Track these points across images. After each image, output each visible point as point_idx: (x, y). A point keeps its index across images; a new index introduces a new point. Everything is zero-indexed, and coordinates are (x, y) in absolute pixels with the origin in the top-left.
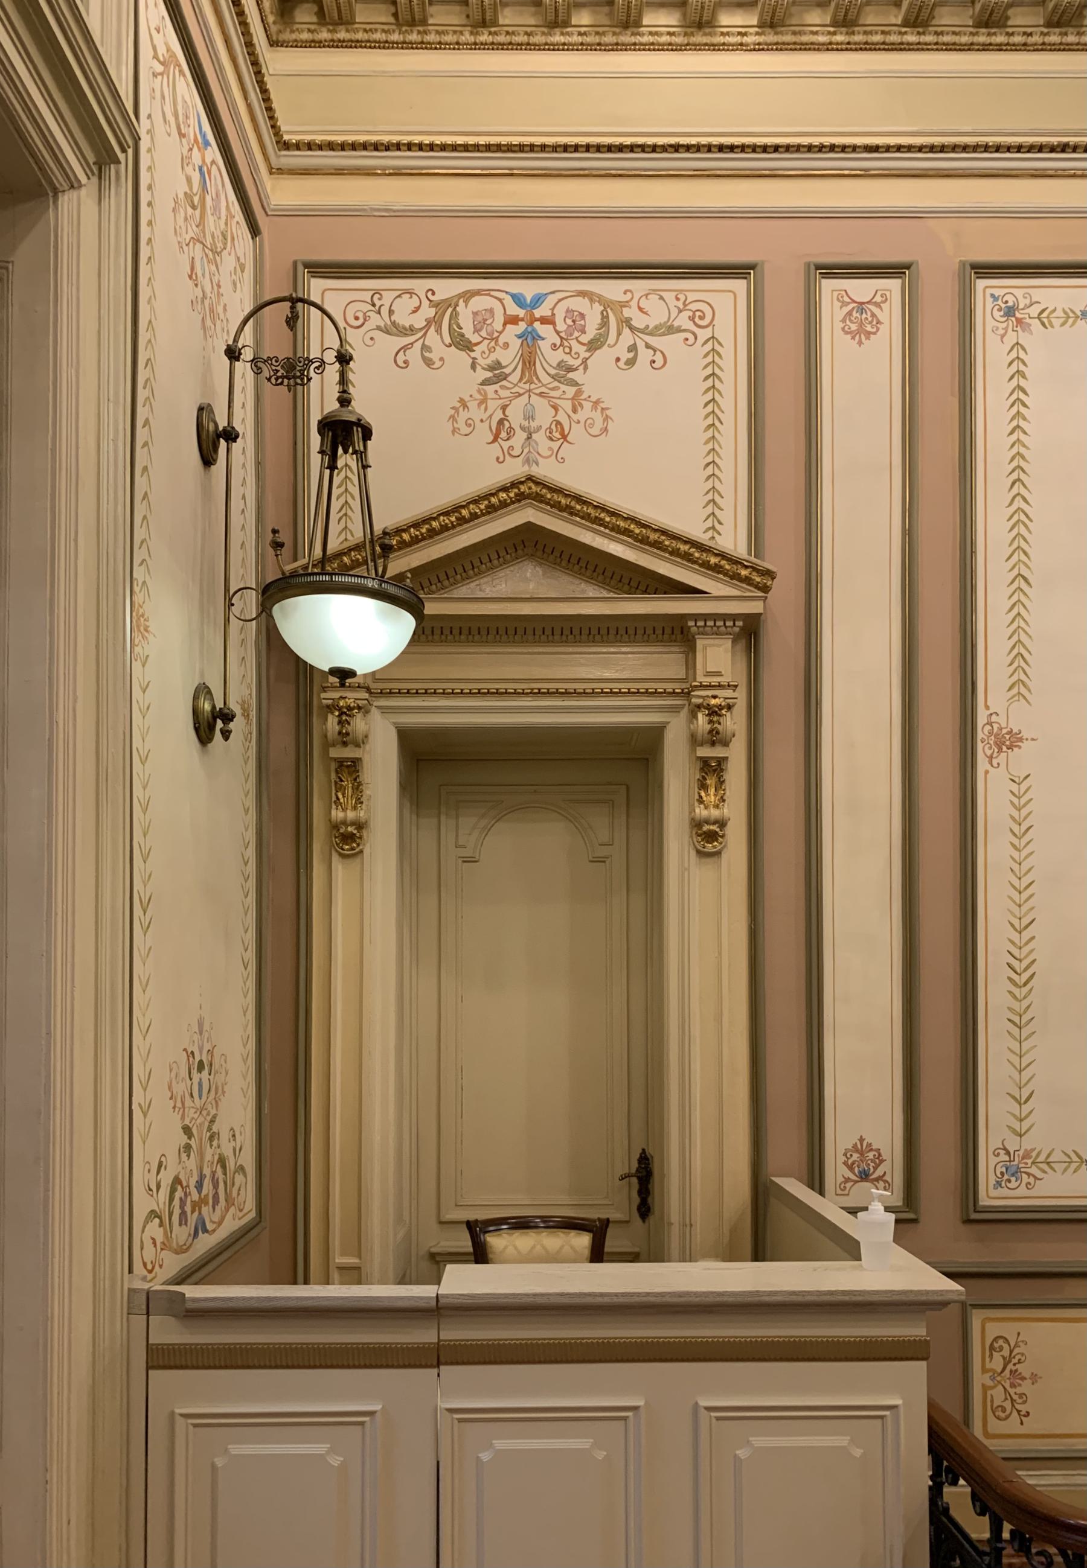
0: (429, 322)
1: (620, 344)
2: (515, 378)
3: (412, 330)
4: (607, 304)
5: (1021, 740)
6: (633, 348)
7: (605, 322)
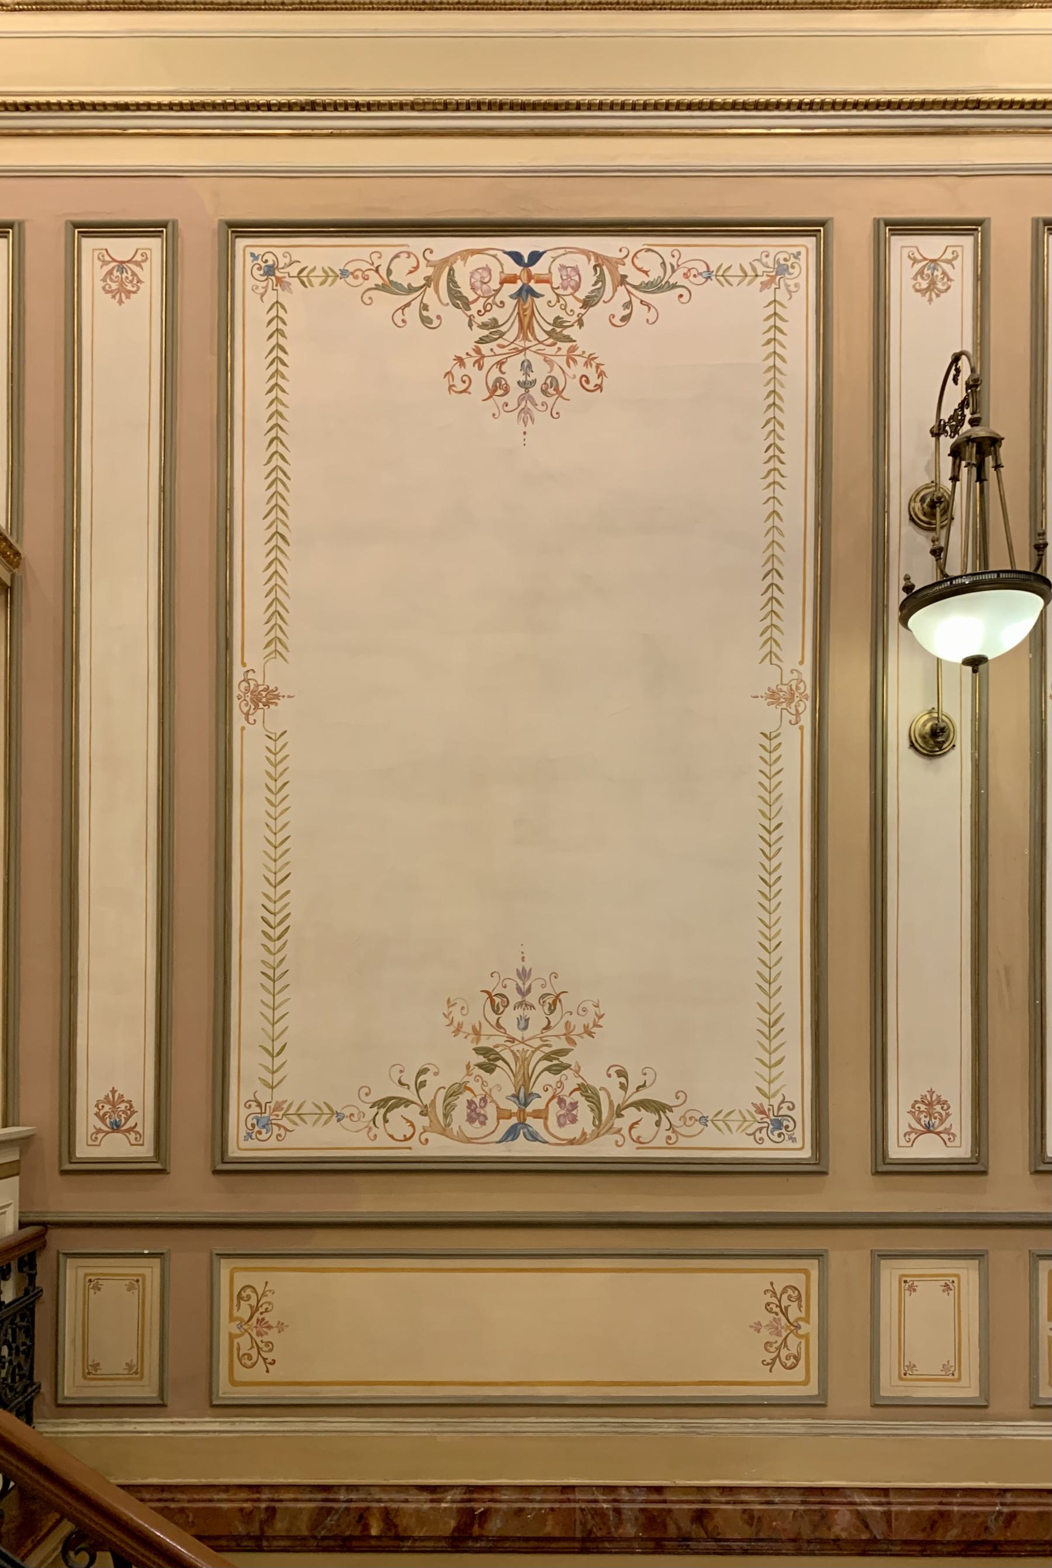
0: (428, 280)
1: (615, 301)
2: (511, 336)
3: (411, 290)
4: (600, 263)
5: (277, 697)
6: (628, 305)
7: (601, 279)
